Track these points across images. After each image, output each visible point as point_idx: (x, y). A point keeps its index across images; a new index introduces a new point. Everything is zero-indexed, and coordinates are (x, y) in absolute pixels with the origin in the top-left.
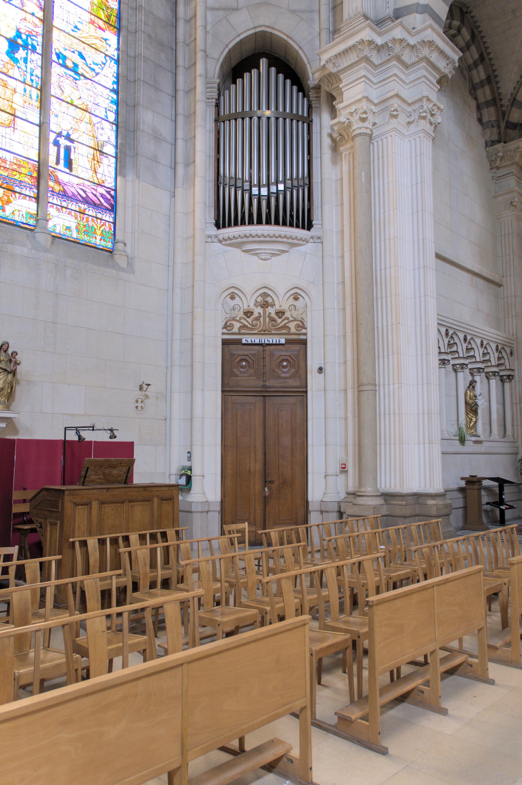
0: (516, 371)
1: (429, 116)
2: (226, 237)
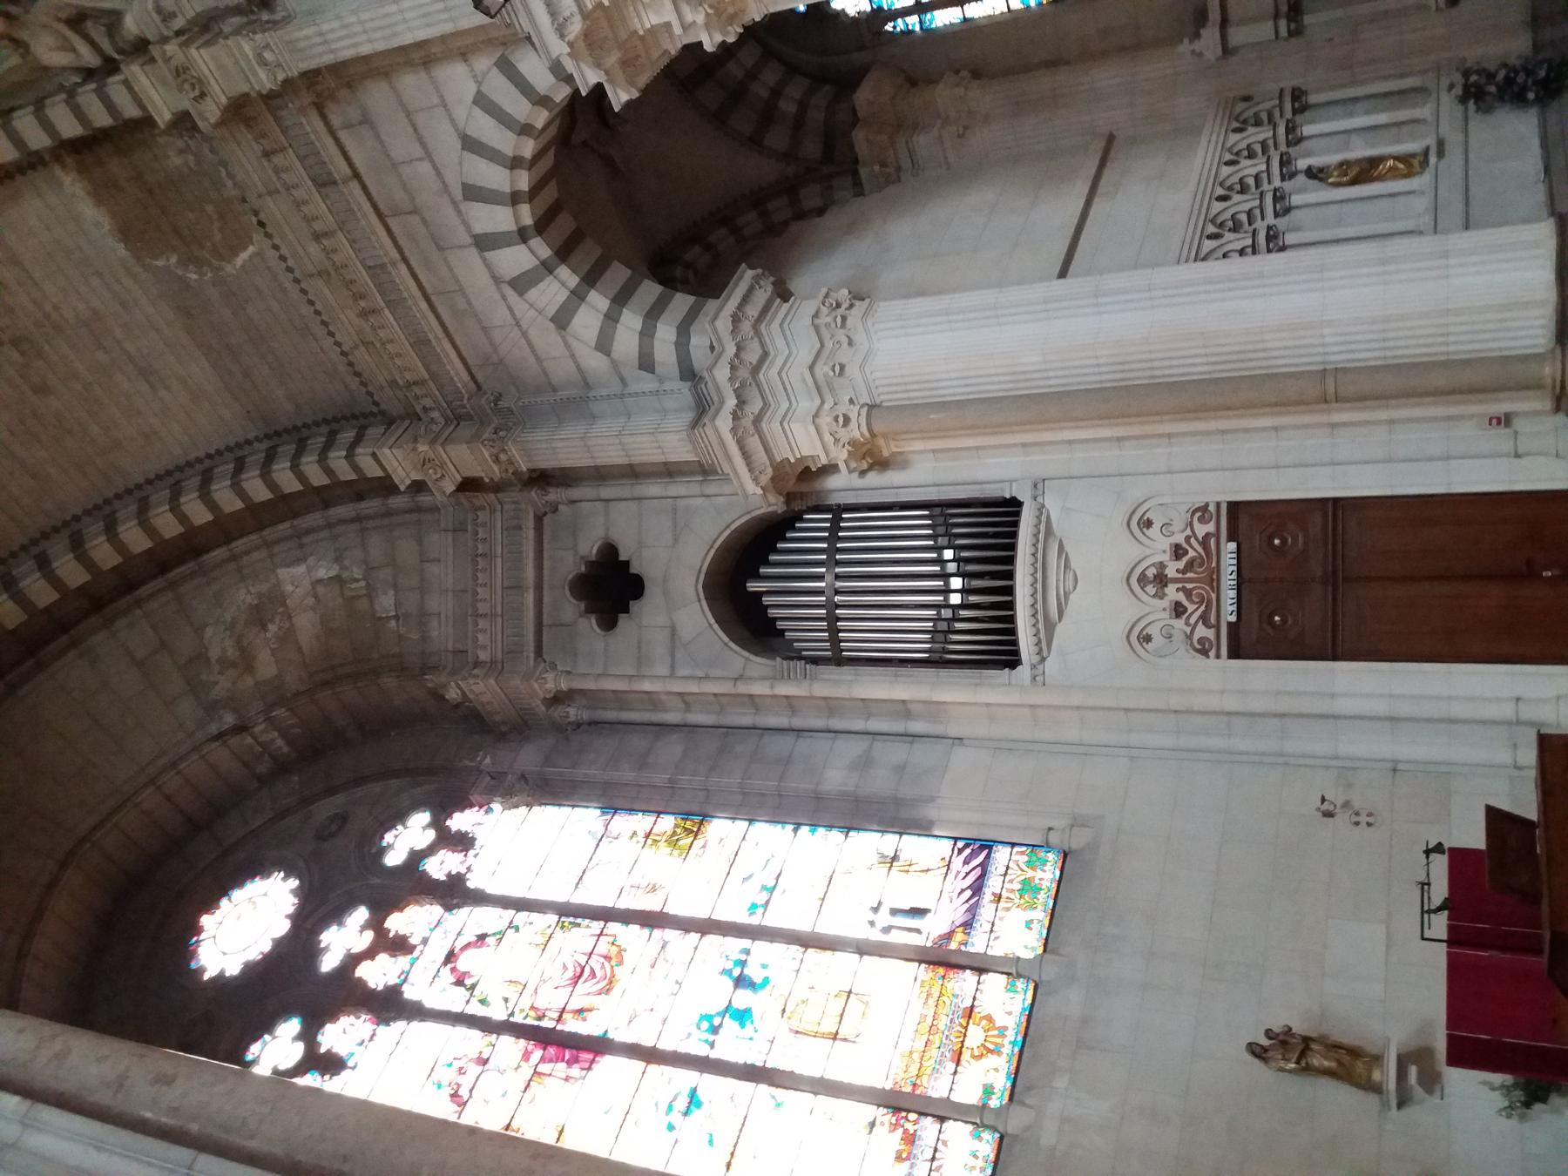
0: (1282, 85)
1: (841, 311)
2: (1036, 649)
